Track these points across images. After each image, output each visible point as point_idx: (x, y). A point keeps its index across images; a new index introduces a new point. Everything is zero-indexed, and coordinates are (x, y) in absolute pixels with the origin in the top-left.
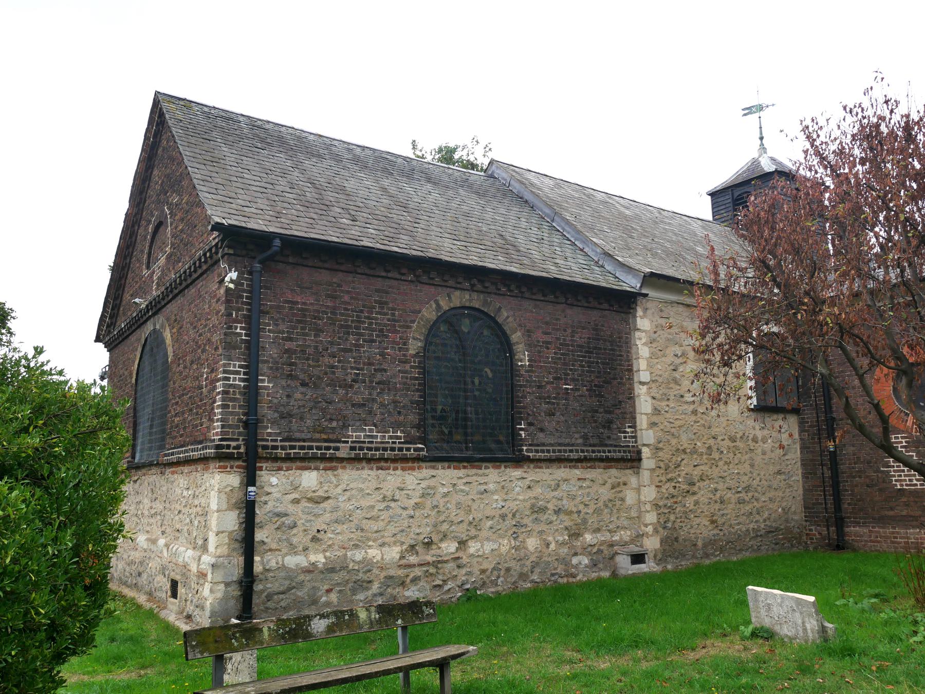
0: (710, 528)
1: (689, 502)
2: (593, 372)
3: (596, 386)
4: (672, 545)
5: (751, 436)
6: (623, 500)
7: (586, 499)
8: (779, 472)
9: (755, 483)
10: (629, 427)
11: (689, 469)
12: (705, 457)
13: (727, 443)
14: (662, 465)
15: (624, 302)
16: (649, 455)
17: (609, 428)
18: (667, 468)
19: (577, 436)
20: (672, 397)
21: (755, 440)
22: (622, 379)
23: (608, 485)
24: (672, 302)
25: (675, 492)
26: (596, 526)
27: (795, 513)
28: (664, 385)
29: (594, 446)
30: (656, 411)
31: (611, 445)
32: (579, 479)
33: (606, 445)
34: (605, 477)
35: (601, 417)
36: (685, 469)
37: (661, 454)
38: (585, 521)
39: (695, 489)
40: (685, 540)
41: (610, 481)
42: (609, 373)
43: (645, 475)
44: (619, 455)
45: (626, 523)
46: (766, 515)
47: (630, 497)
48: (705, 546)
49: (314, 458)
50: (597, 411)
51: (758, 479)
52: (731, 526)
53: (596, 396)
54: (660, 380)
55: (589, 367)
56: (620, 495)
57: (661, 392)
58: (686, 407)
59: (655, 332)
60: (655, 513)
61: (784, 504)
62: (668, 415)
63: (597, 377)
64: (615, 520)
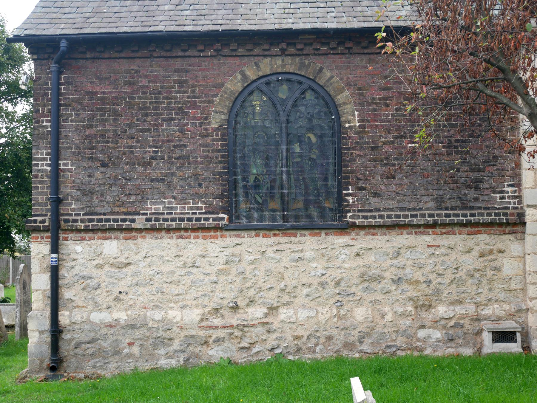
6: (497, 269)
7: (440, 268)
10: (509, 186)
19: (425, 199)
23: (475, 253)
26: (454, 297)
29: (452, 209)
32: (429, 246)
35: (463, 177)
38: (438, 292)
44: (489, 219)
45: (502, 296)
53: (457, 152)
56: (494, 264)
64: (486, 291)
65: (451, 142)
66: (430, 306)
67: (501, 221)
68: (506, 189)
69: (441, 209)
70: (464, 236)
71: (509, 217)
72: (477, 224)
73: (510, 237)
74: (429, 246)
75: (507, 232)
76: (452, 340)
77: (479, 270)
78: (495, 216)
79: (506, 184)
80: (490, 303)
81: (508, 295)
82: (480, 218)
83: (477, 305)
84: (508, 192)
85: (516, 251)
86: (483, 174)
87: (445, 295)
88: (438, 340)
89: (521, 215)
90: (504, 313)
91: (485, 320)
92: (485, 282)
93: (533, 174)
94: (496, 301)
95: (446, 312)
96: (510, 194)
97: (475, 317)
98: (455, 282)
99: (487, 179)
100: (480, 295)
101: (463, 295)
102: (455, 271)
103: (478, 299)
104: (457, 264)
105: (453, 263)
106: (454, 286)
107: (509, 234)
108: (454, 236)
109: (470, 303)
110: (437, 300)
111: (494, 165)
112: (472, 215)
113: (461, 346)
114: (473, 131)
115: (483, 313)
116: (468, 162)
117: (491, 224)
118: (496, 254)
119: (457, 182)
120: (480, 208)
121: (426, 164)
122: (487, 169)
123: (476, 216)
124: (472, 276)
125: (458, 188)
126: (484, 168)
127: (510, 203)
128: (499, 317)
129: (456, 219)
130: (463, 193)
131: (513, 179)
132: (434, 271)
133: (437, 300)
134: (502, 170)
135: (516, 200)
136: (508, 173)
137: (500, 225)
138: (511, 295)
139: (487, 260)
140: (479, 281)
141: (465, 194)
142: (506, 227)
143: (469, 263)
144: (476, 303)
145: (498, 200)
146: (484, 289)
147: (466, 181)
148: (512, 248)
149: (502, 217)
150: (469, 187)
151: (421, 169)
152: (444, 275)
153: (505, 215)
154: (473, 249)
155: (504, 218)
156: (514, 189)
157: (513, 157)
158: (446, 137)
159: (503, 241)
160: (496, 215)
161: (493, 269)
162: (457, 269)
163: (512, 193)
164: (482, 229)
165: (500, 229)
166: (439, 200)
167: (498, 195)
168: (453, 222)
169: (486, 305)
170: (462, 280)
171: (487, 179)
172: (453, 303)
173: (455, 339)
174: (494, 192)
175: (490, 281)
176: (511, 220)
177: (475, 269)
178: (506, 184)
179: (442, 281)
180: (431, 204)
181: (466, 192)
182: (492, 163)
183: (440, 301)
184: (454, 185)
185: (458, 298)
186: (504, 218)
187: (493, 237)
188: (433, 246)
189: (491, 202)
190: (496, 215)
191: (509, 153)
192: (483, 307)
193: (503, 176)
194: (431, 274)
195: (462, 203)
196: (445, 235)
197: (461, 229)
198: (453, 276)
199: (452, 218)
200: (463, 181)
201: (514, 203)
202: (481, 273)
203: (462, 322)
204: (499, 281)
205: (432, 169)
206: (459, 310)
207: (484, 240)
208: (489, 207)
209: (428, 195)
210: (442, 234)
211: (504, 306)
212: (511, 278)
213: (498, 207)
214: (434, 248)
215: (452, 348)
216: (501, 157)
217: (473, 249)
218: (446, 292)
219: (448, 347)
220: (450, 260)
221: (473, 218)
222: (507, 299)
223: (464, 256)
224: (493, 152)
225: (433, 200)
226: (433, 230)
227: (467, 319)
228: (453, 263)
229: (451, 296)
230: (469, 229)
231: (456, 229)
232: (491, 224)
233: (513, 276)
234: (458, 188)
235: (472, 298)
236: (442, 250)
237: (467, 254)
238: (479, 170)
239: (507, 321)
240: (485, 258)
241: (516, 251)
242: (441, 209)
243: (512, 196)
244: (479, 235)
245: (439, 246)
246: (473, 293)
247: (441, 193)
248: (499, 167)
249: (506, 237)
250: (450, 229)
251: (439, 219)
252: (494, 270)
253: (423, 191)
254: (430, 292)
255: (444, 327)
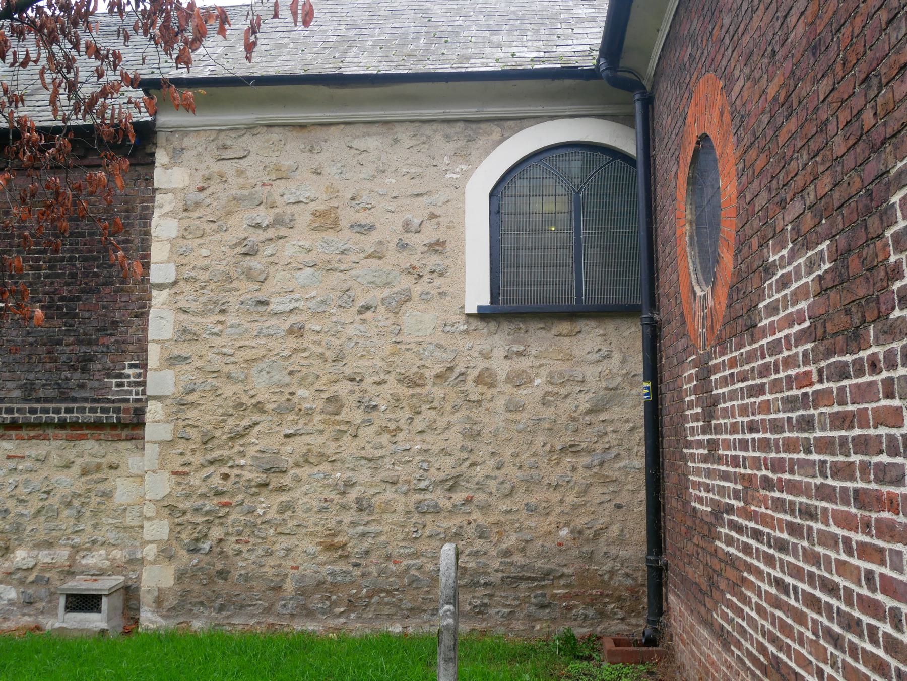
0: (322, 558)
1: (267, 505)
2: (58, 276)
3: (62, 299)
4: (209, 581)
5: (473, 374)
6: (107, 495)
7: (22, 491)
8: (571, 449)
9: (479, 472)
10: (131, 366)
11: (273, 443)
12: (318, 418)
13: (392, 387)
14: (193, 433)
15: (137, 146)
16: (160, 416)
17: (84, 370)
18: (207, 440)
19: (10, 385)
20: (234, 305)
21: (486, 379)
22: (124, 281)
23: (76, 470)
24: (250, 128)
25: (228, 486)
26: (42, 536)
27: (621, 540)
28: (212, 286)
29: (47, 400)
30: (186, 335)
31: (86, 400)
32: (9, 457)
33: (74, 400)
34: (71, 453)
35: (65, 352)
36: (256, 442)
37: (192, 414)
38: (18, 529)
39: (286, 480)
40: (247, 578)
41: (79, 461)
42: (97, 275)
43: (151, 450)
44: (90, 417)
45: (111, 536)
46: (511, 540)
47: (123, 491)
48: (303, 592)
49: (49, 424)
50: (60, 343)
51: (491, 463)
52: (389, 557)
53: (62, 316)
54: (204, 276)
55: (50, 268)
56: (101, 487)
57: (203, 299)
58: (274, 321)
59: (201, 190)
60: (166, 522)
61: (580, 521)
62: (218, 341)
63: (67, 284)
64: (89, 529)
65: (53, 300)
66: (7, 548)
67: (110, 421)
68: (127, 371)
69: (30, 400)
70: (61, 442)
71: (122, 415)
72: (76, 425)
73: (129, 445)
74: (9, 457)
75: (124, 437)
76: (31, 603)
77: (80, 495)
78: (101, 412)
79: (127, 363)
80: (95, 546)
81: (121, 535)
82: (79, 415)
83: (76, 549)
84: (128, 377)
85: (135, 467)
86: (94, 348)
87: (27, 532)
88: (11, 603)
89: (140, 413)
90: (108, 563)
91: (82, 573)
92: (88, 514)
93: (159, 349)
94: (103, 544)
95: (24, 559)
96: (132, 379)
97: (66, 568)
98: (44, 512)
99: (100, 356)
100: (80, 534)
101: (54, 533)
102: (45, 496)
103: (77, 540)
104: (48, 485)
105: (42, 483)
106: (43, 519)
107: (127, 440)
108: (47, 442)
109: (65, 545)
110: (16, 540)
111: (111, 335)
112: (68, 411)
113: (42, 613)
114: (86, 283)
115: (84, 562)
116: (75, 331)
117: (97, 425)
118: (107, 470)
119: (56, 361)
120: (86, 400)
121: (14, 334)
122: (101, 342)
123: (73, 412)
124: (69, 504)
125: (58, 369)
126: (97, 340)
127: (130, 393)
128: (101, 569)
129: (44, 416)
130: (63, 377)
131: (138, 356)
132: (12, 496)
133: (16, 540)
134: (123, 343)
135: (140, 389)
136: (131, 347)
137: (113, 426)
138: (125, 535)
139: (92, 480)
140: (79, 512)
141: (66, 379)
142: (123, 429)
143: (65, 484)
144: (73, 547)
145: (114, 389)
146: (86, 525)
147: (69, 358)
148: (130, 462)
149: (111, 414)
150: (73, 369)
151: (7, 341)
152: (27, 501)
153: (117, 410)
154: (73, 462)
155: (115, 415)
156: (138, 371)
157: (140, 323)
158: (47, 293)
159: (117, 451)
160: (103, 410)
161: (100, 494)
162: (48, 492)
163: (134, 377)
164: (87, 432)
165: (114, 432)
166: (29, 387)
167: (114, 381)
168: (39, 421)
169: (89, 549)
170: (53, 511)
171: (100, 356)
172: (39, 546)
173: (36, 602)
174: (109, 376)
175: (95, 513)
176: (125, 418)
177: (74, 493)
178: (127, 363)
179: (23, 512)
180: (17, 394)
181: (69, 375)
182: (109, 332)
183: (20, 542)
184: (52, 364)
185: (47, 538)
186: (115, 415)
187: (104, 445)
188: (15, 457)
189: (103, 391)
190: (103, 410)
191: (136, 317)
192: (85, 553)
193: (123, 351)
194: (9, 500)
195: (62, 393)
196: (34, 441)
197: (57, 432)
198: (41, 504)
199: (39, 415)
200: (65, 359)
201: (137, 394)
202: (83, 499)
203: (47, 575)
204: (108, 513)
205: (23, 341)
206: (44, 556)
207: (90, 449)
208: (100, 399)
209: (13, 380)
210: (31, 438)
211: (114, 552)
212: (125, 509)
213: (113, 398)
214: (16, 460)
215: (30, 615)
216: (122, 322)
217: (73, 462)
218: (29, 528)
219: (24, 615)
220: (37, 480)
221: (68, 415)
222: (119, 541)
223: (59, 473)
224: (112, 315)
225: (19, 388)
226: (17, 432)
227: (54, 571)
228: (42, 483)
229: (37, 534)
230: (69, 432)
231: (50, 432)
232: (97, 425)
233: (129, 505)
234: (58, 369)
235: (68, 539)
236: (28, 464)
237: (66, 471)
238: (89, 343)
239: (114, 577)
240: (90, 477)
241: (135, 467)
242: (30, 400)
243: (134, 382)
244: (83, 442)
245: (23, 458)
246: (69, 531)
247: (32, 376)
248: (119, 338)
249: (123, 445)
250: (41, 432)
251: (21, 416)
252: (101, 496)
253: (8, 374)
254: (7, 527)
255: (22, 582)
